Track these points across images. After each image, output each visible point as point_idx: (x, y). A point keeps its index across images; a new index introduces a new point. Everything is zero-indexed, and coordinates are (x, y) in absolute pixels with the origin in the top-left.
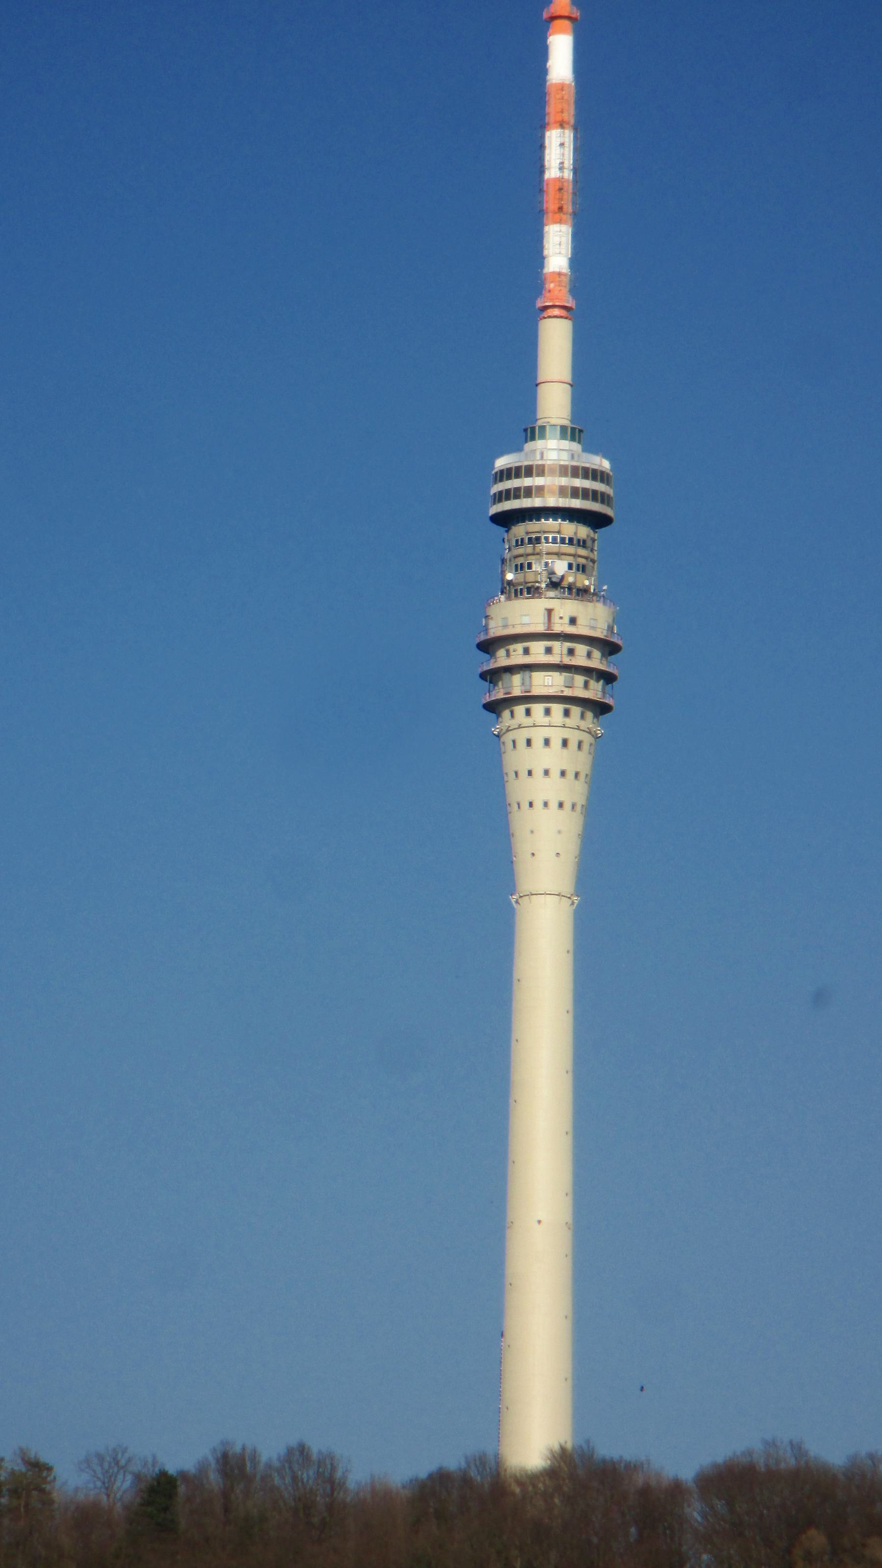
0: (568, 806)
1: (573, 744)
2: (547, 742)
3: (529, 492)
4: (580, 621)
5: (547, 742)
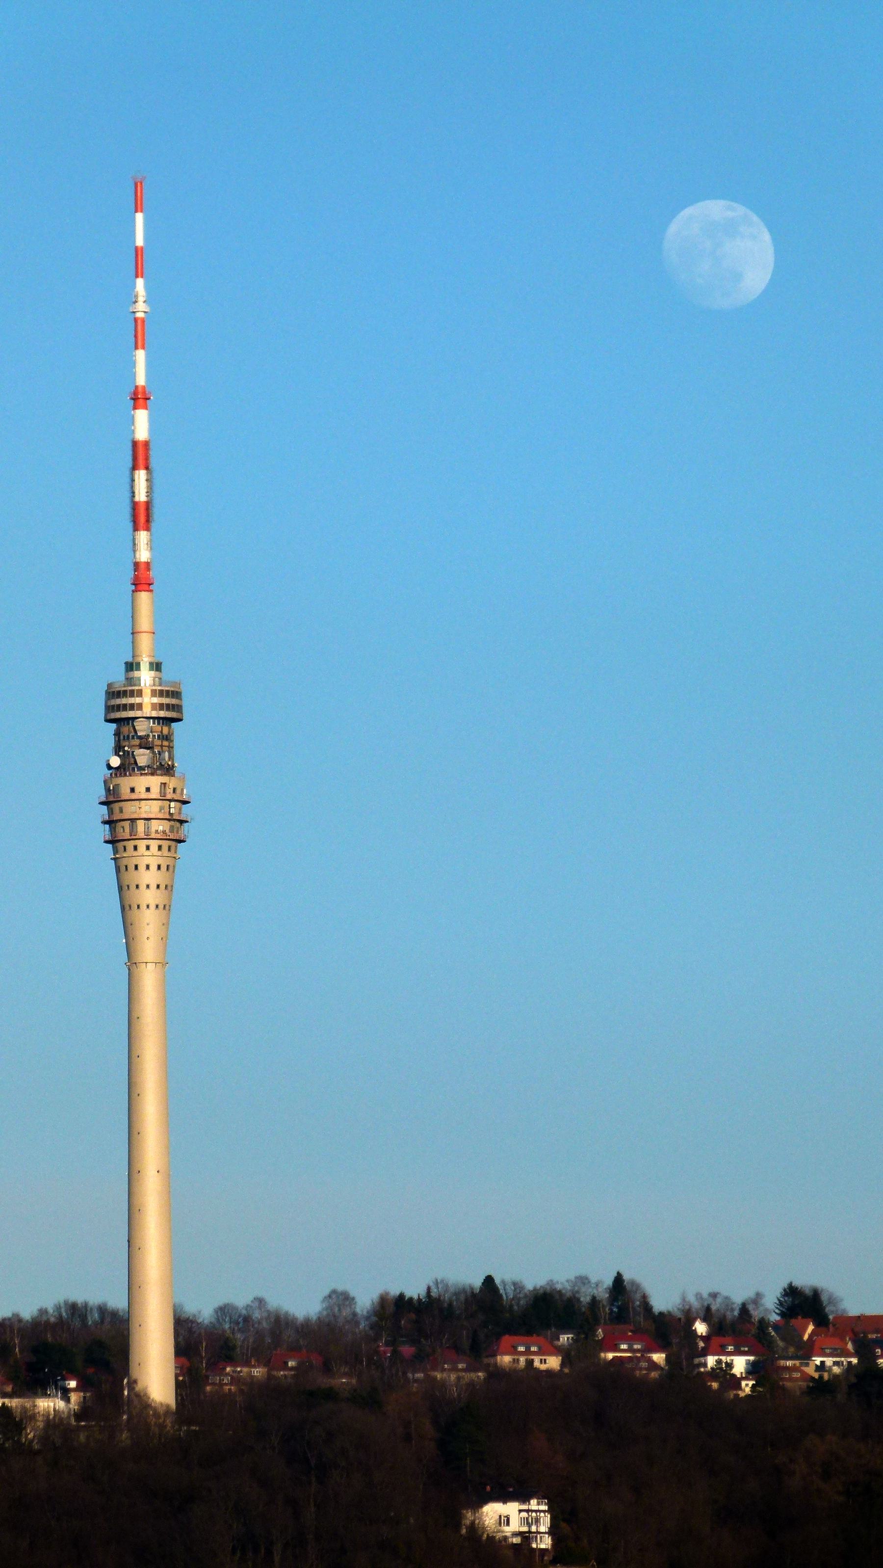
0: (162, 887)
1: (164, 868)
2: (148, 867)
3: (125, 707)
4: (136, 790)
5: (148, 867)
